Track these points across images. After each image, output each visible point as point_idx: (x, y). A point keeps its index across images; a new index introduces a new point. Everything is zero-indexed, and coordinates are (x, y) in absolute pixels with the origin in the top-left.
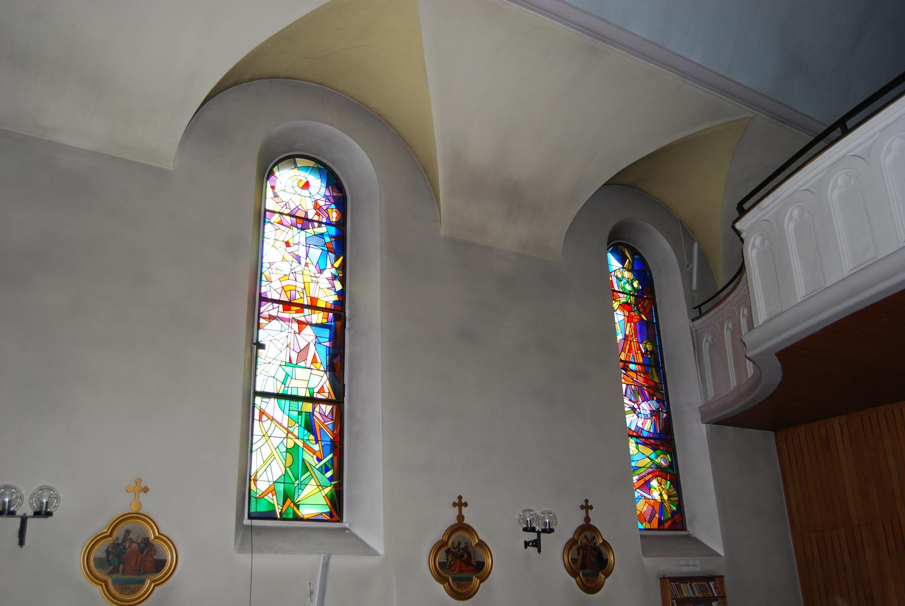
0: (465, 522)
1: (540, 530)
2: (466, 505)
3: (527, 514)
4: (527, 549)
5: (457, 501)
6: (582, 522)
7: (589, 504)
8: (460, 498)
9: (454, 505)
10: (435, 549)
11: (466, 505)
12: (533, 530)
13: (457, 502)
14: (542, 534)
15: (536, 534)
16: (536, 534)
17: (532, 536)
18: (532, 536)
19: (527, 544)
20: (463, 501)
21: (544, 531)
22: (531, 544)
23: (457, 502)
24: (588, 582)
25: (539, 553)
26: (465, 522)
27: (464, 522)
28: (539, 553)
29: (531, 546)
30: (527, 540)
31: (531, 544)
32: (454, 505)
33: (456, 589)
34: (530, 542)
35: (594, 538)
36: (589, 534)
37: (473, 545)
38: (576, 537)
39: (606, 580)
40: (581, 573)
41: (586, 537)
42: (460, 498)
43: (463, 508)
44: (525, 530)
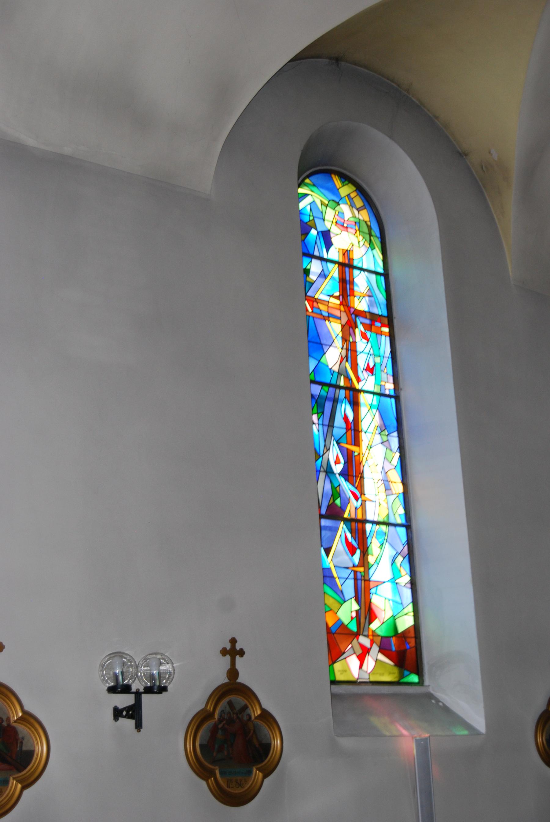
0: (239, 680)
1: (142, 690)
2: (242, 653)
3: (117, 661)
4: (118, 721)
5: (228, 647)
6: (222, 679)
7: (238, 647)
8: (233, 641)
9: (224, 652)
10: (195, 724)
11: (242, 653)
12: (126, 689)
13: (228, 649)
14: (146, 698)
15: (133, 695)
16: (133, 695)
17: (127, 700)
18: (127, 700)
19: (118, 713)
20: (238, 647)
21: (149, 690)
22: (124, 713)
23: (228, 649)
24: (228, 786)
25: (139, 731)
26: (239, 680)
27: (238, 681)
28: (139, 731)
29: (125, 717)
30: (120, 707)
31: (124, 713)
32: (224, 652)
33: (226, 788)
34: (124, 709)
35: (245, 708)
36: (239, 700)
37: (253, 717)
38: (210, 708)
39: (266, 781)
40: (217, 772)
41: (230, 703)
42: (233, 641)
43: (238, 658)
44: (112, 690)
